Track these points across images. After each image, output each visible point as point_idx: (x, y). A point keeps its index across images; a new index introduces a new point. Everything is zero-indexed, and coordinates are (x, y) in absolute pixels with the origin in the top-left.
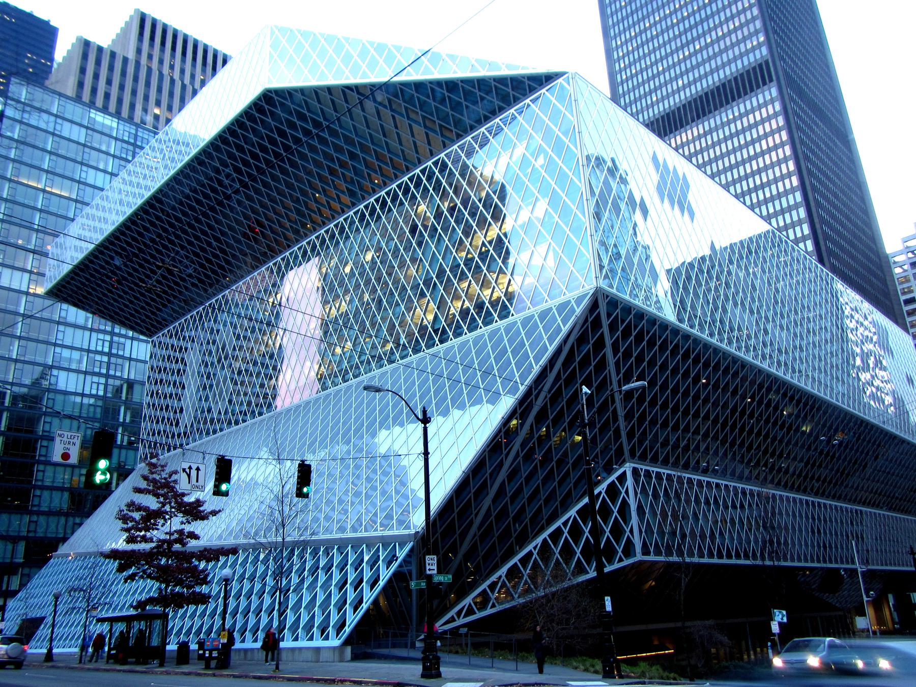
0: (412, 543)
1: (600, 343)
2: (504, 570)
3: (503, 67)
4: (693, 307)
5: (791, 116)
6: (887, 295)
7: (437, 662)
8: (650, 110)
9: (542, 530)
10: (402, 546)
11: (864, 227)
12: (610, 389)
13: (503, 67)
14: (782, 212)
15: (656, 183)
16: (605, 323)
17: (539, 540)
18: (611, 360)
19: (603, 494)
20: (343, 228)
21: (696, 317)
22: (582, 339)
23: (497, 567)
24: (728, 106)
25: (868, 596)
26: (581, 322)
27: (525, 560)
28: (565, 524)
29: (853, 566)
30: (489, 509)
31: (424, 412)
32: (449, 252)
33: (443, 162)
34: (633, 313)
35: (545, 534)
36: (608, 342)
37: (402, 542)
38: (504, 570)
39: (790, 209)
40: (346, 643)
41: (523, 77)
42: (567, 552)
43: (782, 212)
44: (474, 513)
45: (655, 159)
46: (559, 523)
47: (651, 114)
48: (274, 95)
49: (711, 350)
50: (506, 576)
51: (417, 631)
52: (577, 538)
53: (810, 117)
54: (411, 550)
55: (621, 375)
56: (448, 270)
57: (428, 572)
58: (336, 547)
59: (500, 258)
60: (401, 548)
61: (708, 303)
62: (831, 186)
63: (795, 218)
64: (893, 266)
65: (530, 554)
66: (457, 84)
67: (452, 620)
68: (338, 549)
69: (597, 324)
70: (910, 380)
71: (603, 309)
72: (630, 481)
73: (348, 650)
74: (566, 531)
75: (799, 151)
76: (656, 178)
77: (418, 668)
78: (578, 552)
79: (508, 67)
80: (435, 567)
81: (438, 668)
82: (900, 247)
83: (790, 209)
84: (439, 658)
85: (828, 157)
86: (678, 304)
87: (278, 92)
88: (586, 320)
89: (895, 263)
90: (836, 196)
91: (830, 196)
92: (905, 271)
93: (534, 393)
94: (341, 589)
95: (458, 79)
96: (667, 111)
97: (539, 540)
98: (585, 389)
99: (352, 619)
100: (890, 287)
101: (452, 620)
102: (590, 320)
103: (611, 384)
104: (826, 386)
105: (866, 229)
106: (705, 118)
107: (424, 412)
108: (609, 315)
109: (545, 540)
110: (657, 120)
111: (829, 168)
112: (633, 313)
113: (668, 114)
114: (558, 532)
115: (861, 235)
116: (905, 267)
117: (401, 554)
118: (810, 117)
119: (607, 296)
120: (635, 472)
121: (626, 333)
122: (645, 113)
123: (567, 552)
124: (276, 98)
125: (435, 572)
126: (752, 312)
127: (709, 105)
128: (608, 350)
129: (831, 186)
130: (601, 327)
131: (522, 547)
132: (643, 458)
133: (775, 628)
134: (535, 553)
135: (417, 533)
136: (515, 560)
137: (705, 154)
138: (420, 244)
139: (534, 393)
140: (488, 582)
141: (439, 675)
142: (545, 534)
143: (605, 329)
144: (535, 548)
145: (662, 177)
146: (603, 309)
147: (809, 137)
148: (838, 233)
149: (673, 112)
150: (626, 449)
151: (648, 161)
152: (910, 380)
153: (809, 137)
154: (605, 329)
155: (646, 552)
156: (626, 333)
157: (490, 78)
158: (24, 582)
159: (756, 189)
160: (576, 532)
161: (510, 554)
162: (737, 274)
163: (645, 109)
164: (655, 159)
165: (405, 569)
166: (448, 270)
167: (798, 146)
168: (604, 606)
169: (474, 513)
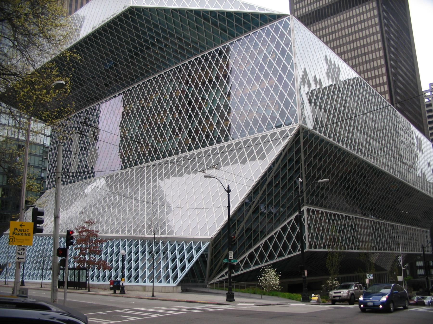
0: (209, 242)
1: (298, 151)
2: (247, 254)
3: (257, 9)
4: (340, 133)
5: (382, 18)
6: (422, 122)
7: (233, 297)
8: (310, 7)
9: (265, 236)
10: (204, 244)
11: (413, 79)
12: (301, 172)
13: (257, 9)
14: (365, 54)
15: (326, 70)
16: (302, 141)
17: (263, 241)
18: (303, 159)
19: (293, 220)
20: (163, 78)
21: (340, 137)
22: (290, 150)
23: (244, 253)
24: (351, 9)
25: (404, 267)
26: (291, 141)
27: (256, 250)
28: (275, 234)
29: (398, 252)
30: (243, 227)
31: (228, 187)
32: (222, 98)
33: (221, 50)
34: (314, 136)
35: (266, 239)
36: (302, 150)
37: (204, 241)
38: (247, 254)
39: (378, 67)
40: (178, 285)
41: (267, 14)
42: (276, 247)
43: (365, 54)
44: (237, 229)
45: (326, 58)
46: (272, 233)
47: (310, 9)
48: (135, 10)
49: (342, 151)
50: (248, 257)
51: (208, 280)
52: (280, 241)
53: (391, 18)
54: (209, 245)
55: (306, 166)
56: (222, 107)
57: (230, 258)
58: (168, 241)
59: (250, 104)
60: (203, 244)
61: (346, 130)
62: (399, 56)
63: (380, 73)
64: (424, 98)
65: (259, 247)
66: (232, 15)
67: (223, 276)
68: (169, 242)
69: (298, 142)
70: (429, 165)
71: (301, 135)
72: (305, 216)
73: (179, 288)
74: (276, 237)
75: (385, 38)
76: (326, 68)
77: (225, 298)
78: (281, 247)
79: (260, 8)
80: (232, 256)
81: (234, 298)
82: (428, 88)
83: (378, 67)
84: (234, 294)
85: (399, 41)
86: (333, 131)
87: (138, 9)
88: (294, 140)
89: (425, 96)
90: (400, 62)
91: (398, 62)
92: (430, 101)
93: (268, 174)
94: (136, 254)
95: (233, 12)
96: (318, 8)
97: (263, 241)
98: (300, 179)
99: (181, 276)
100: (422, 111)
101: (223, 276)
102: (295, 140)
103: (302, 170)
104: (393, 169)
105: (414, 80)
106: (338, 14)
107: (228, 187)
108: (304, 138)
109: (266, 241)
110: (313, 12)
111: (399, 47)
112: (314, 136)
113: (319, 10)
114: (272, 237)
115: (411, 83)
116: (430, 99)
117: (203, 248)
118: (391, 18)
119: (304, 129)
120: (308, 210)
121: (310, 146)
122: (307, 8)
123: (276, 247)
124: (135, 11)
125: (232, 258)
126: (364, 134)
127: (340, 8)
128: (302, 154)
129: (399, 56)
130: (300, 143)
131: (255, 244)
132: (312, 204)
133: (367, 281)
134: (261, 247)
135: (212, 238)
136: (252, 250)
137: (337, 34)
138: (206, 91)
139: (268, 174)
140: (240, 260)
141: (234, 300)
142: (266, 239)
143: (302, 145)
144: (261, 245)
145: (329, 68)
146: (301, 135)
147: (390, 30)
148: (400, 81)
149: (322, 9)
150: (305, 199)
151: (323, 59)
152: (429, 165)
153: (390, 30)
154: (302, 145)
155: (310, 247)
156: (310, 146)
157: (250, 13)
158: (152, 275)
159: (348, 27)
160: (280, 237)
161: (250, 247)
162: (349, 102)
163: (306, 6)
164: (326, 58)
165: (205, 253)
166: (222, 107)
167: (385, 35)
168: (304, 274)
169: (237, 229)
